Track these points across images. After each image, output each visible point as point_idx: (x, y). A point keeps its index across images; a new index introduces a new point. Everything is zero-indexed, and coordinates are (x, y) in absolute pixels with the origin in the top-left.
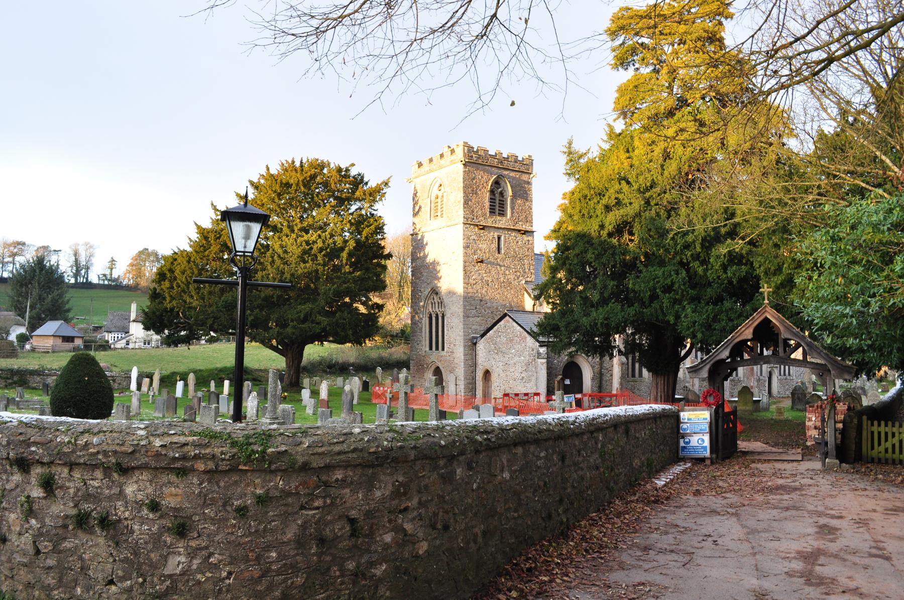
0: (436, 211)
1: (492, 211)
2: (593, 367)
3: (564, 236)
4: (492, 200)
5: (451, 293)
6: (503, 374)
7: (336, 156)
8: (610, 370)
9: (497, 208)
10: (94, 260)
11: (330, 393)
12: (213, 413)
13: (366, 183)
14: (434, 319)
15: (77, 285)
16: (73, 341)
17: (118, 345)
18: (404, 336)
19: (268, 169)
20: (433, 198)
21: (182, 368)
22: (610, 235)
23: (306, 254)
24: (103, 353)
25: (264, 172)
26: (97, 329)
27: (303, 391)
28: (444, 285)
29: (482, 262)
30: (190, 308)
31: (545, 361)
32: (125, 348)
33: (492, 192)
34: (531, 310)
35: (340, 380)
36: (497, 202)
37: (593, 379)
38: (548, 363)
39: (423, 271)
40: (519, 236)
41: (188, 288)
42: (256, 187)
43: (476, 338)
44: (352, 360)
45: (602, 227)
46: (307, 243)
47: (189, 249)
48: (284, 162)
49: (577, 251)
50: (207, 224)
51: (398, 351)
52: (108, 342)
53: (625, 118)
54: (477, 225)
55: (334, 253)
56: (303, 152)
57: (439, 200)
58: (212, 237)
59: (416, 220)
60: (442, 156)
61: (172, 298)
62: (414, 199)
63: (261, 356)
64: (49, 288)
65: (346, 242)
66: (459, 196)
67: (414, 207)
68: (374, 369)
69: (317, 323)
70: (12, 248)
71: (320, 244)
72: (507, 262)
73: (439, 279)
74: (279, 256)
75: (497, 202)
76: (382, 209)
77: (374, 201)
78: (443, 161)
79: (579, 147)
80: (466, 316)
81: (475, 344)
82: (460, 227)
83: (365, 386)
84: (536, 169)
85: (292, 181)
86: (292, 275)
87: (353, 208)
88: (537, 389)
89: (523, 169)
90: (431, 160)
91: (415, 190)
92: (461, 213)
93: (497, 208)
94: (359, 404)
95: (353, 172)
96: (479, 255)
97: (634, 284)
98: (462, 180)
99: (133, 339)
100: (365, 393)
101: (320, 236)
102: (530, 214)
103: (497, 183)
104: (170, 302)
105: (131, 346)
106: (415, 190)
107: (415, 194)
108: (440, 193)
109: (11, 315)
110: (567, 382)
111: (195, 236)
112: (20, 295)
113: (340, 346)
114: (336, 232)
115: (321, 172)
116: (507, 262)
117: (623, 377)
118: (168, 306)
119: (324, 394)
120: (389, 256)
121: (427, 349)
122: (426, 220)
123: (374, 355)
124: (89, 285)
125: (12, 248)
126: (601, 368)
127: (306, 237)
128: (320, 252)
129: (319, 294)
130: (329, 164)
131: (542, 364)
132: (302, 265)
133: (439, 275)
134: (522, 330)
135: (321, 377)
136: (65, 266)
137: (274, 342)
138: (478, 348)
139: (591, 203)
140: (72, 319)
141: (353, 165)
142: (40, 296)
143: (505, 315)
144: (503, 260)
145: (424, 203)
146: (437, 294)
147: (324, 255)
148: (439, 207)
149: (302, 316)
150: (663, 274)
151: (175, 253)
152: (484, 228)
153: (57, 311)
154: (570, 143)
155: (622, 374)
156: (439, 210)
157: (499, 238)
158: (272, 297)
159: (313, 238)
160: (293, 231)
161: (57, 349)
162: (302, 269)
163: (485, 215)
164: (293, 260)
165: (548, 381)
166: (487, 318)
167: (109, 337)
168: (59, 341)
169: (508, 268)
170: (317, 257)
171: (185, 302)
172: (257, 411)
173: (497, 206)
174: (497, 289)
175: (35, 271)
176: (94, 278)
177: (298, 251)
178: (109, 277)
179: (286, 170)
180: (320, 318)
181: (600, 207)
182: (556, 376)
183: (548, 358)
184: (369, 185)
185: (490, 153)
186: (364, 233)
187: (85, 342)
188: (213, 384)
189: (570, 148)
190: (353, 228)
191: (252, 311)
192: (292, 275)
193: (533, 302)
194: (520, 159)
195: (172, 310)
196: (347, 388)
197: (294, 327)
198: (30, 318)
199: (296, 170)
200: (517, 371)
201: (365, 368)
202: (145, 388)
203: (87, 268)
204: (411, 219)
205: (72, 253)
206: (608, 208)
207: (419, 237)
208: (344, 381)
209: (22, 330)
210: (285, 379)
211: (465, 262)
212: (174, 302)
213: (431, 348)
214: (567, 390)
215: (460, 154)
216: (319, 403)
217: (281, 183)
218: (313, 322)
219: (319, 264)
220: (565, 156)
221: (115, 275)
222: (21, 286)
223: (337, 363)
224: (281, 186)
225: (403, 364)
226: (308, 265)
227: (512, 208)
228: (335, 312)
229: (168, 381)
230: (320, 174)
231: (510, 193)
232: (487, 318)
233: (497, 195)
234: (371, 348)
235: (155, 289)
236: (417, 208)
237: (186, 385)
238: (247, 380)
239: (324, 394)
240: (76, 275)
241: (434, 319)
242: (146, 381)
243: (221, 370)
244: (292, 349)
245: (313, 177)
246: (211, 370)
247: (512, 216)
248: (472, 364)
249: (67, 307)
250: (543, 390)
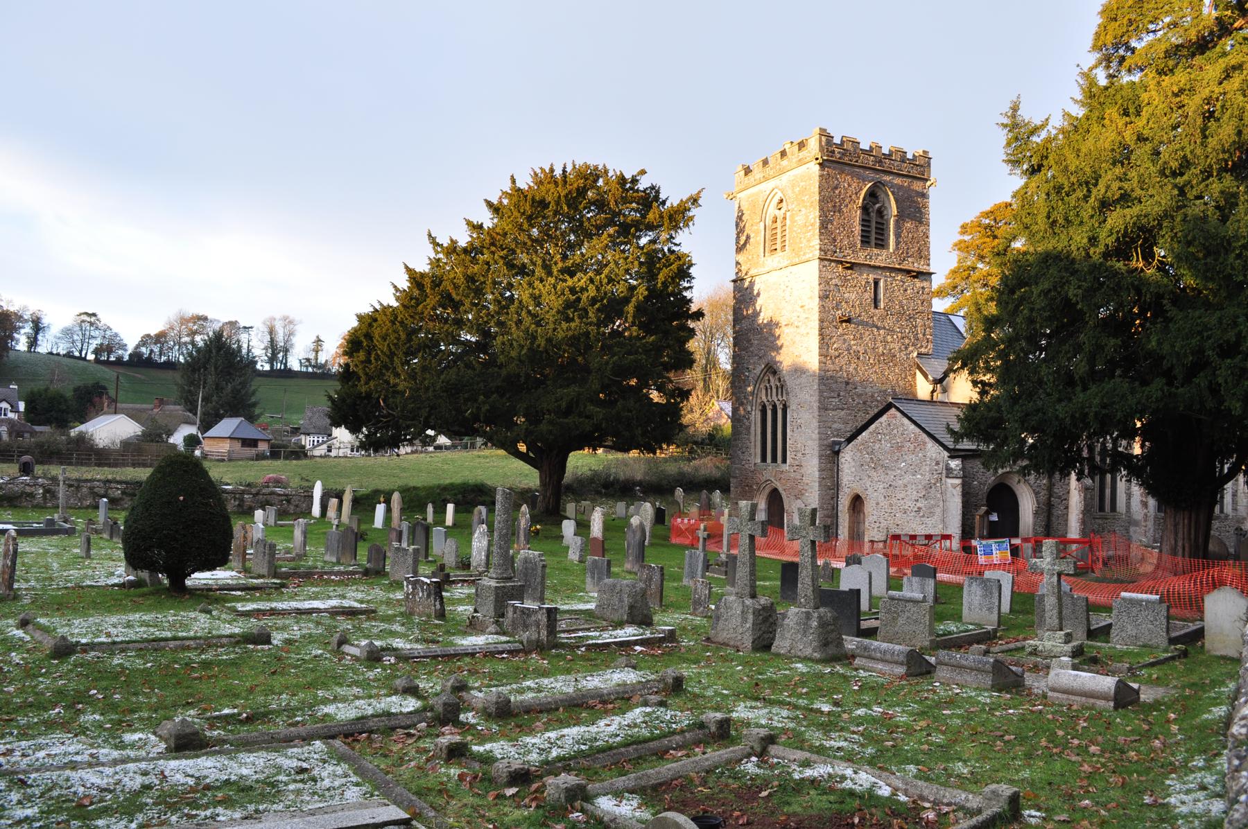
0: (774, 243)
1: (865, 241)
2: (1036, 493)
3: (1016, 261)
4: (865, 222)
5: (799, 371)
6: (884, 503)
7: (618, 161)
8: (1065, 499)
9: (873, 236)
10: (294, 340)
11: (607, 527)
12: (410, 561)
13: (664, 203)
14: (769, 413)
15: (272, 373)
16: (256, 446)
17: (317, 452)
18: (713, 441)
19: (514, 181)
20: (769, 222)
21: (383, 484)
22: (1106, 255)
23: (571, 306)
24: (295, 462)
25: (507, 187)
26: (296, 431)
27: (565, 523)
28: (785, 359)
29: (849, 321)
30: (394, 392)
31: (958, 481)
32: (326, 456)
33: (865, 209)
34: (928, 397)
35: (620, 507)
36: (873, 225)
37: (1036, 514)
38: (963, 485)
39: (752, 337)
40: (909, 281)
41: (392, 362)
42: (495, 209)
43: (840, 443)
44: (639, 477)
45: (1093, 240)
46: (573, 290)
47: (395, 304)
48: (538, 171)
49: (1045, 285)
50: (422, 267)
51: (707, 465)
52: (304, 447)
53: (1108, 67)
54: (841, 262)
55: (613, 307)
56: (565, 155)
57: (779, 224)
58: (427, 283)
59: (741, 258)
60: (783, 154)
61: (369, 378)
62: (737, 225)
63: (502, 468)
64: (230, 374)
65: (632, 289)
66: (813, 215)
67: (738, 238)
68: (671, 491)
69: (588, 417)
70: (191, 325)
71: (592, 292)
72: (889, 322)
73: (778, 349)
74: (529, 312)
75: (873, 225)
76: (685, 241)
77: (676, 228)
78: (785, 163)
79: (1031, 114)
80: (823, 408)
81: (837, 453)
82: (816, 264)
83: (660, 517)
84: (935, 172)
85: (549, 199)
86: (549, 340)
87: (644, 241)
88: (945, 527)
89: (914, 172)
90: (765, 162)
91: (740, 210)
92: (816, 242)
93: (873, 236)
94: (651, 545)
95: (643, 184)
96: (845, 310)
97: (1159, 343)
98: (817, 190)
99: (336, 443)
100: (659, 527)
101: (592, 281)
102: (926, 245)
103: (872, 195)
104: (366, 383)
105: (333, 453)
106: (740, 210)
107: (740, 218)
108: (780, 214)
109: (178, 409)
110: (994, 517)
111: (404, 284)
112: (191, 383)
113: (620, 455)
114: (617, 275)
115: (593, 185)
116: (889, 322)
117: (1087, 511)
118: (363, 390)
119: (596, 529)
120: (699, 315)
121: (759, 460)
122: (760, 261)
123: (672, 469)
124: (288, 373)
125: (191, 325)
126: (1050, 496)
127: (570, 282)
128: (593, 305)
129: (589, 372)
130: (606, 172)
131: (954, 487)
132: (564, 325)
133: (779, 343)
134: (918, 430)
135: (593, 501)
136: (256, 346)
137: (522, 448)
138: (842, 460)
139: (1072, 200)
140: (259, 416)
141: (643, 172)
142: (217, 385)
143: (889, 406)
144: (883, 318)
145: (756, 231)
146: (775, 373)
147: (598, 310)
148: (779, 236)
149: (564, 405)
150: (1220, 320)
151: (376, 310)
152: (852, 266)
153: (240, 406)
154: (1015, 109)
155: (1086, 506)
156: (779, 241)
157: (876, 283)
158: (519, 376)
159: (582, 283)
160: (550, 274)
161: (234, 456)
162: (564, 330)
163: (855, 246)
164: (550, 317)
165: (964, 515)
166: (858, 409)
167: (307, 441)
168: (238, 445)
169: (891, 331)
170: (587, 313)
171: (388, 382)
172: (488, 556)
173: (874, 233)
174: (873, 365)
175: (210, 351)
176: (294, 364)
177: (556, 303)
178: (313, 362)
179: (541, 183)
180: (591, 408)
181: (1087, 210)
182: (977, 507)
183: (964, 477)
184: (668, 204)
185: (862, 146)
186: (661, 277)
187: (272, 446)
188: (430, 508)
189: (1014, 116)
190: (644, 269)
191: (487, 397)
192: (549, 340)
193: (931, 387)
194: (909, 156)
195: (369, 395)
196: (635, 521)
197: (551, 422)
198: (204, 414)
199: (556, 183)
200: (909, 498)
201: (658, 488)
202: (331, 513)
203: (286, 351)
204: (732, 256)
205: (266, 330)
206: (1105, 205)
207: (746, 284)
208: (627, 508)
209: (192, 430)
210: (539, 505)
211: (822, 321)
212: (372, 383)
213: (764, 459)
214: (994, 532)
215: (814, 146)
216: (591, 545)
217: (533, 199)
218: (580, 415)
219: (590, 324)
220: (1006, 131)
221: (322, 359)
222: (194, 371)
223: (617, 481)
224: (532, 206)
225: (711, 484)
226: (573, 325)
227: (898, 236)
228: (616, 401)
229: (363, 504)
230: (592, 187)
231: (895, 212)
232: (858, 409)
233: (873, 215)
234: (666, 461)
235: (347, 365)
236: (743, 239)
237: (389, 510)
238: (482, 504)
239: (596, 529)
240: (272, 360)
241: (769, 413)
242: (334, 502)
243: (445, 489)
244: (548, 457)
245: (582, 192)
246: (431, 488)
247: (897, 248)
248: (831, 483)
249: (253, 400)
250: (955, 528)
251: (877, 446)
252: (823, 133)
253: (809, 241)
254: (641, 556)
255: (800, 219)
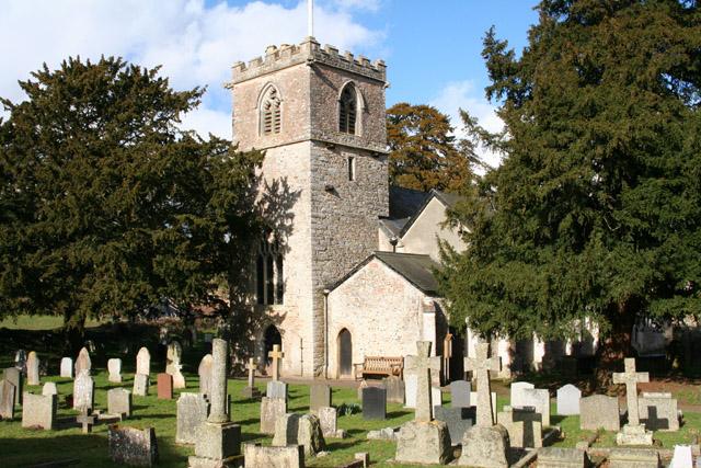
1: (343, 129)
4: (343, 113)
33: (341, 102)
48: (507, 50)
89: (375, 76)
98: (308, 85)
152: (333, 147)
154: (490, 35)
227: (364, 122)
233: (347, 107)
251: (361, 289)
252: (313, 42)
253: (301, 125)
254: (645, 261)
255: (293, 108)
